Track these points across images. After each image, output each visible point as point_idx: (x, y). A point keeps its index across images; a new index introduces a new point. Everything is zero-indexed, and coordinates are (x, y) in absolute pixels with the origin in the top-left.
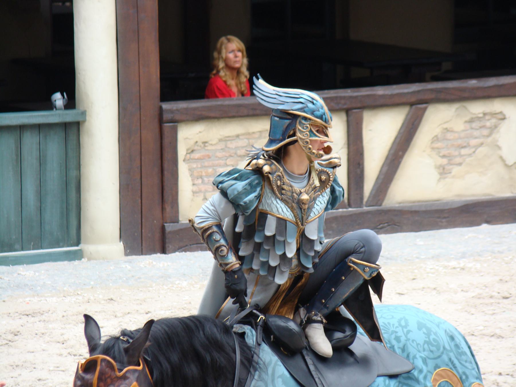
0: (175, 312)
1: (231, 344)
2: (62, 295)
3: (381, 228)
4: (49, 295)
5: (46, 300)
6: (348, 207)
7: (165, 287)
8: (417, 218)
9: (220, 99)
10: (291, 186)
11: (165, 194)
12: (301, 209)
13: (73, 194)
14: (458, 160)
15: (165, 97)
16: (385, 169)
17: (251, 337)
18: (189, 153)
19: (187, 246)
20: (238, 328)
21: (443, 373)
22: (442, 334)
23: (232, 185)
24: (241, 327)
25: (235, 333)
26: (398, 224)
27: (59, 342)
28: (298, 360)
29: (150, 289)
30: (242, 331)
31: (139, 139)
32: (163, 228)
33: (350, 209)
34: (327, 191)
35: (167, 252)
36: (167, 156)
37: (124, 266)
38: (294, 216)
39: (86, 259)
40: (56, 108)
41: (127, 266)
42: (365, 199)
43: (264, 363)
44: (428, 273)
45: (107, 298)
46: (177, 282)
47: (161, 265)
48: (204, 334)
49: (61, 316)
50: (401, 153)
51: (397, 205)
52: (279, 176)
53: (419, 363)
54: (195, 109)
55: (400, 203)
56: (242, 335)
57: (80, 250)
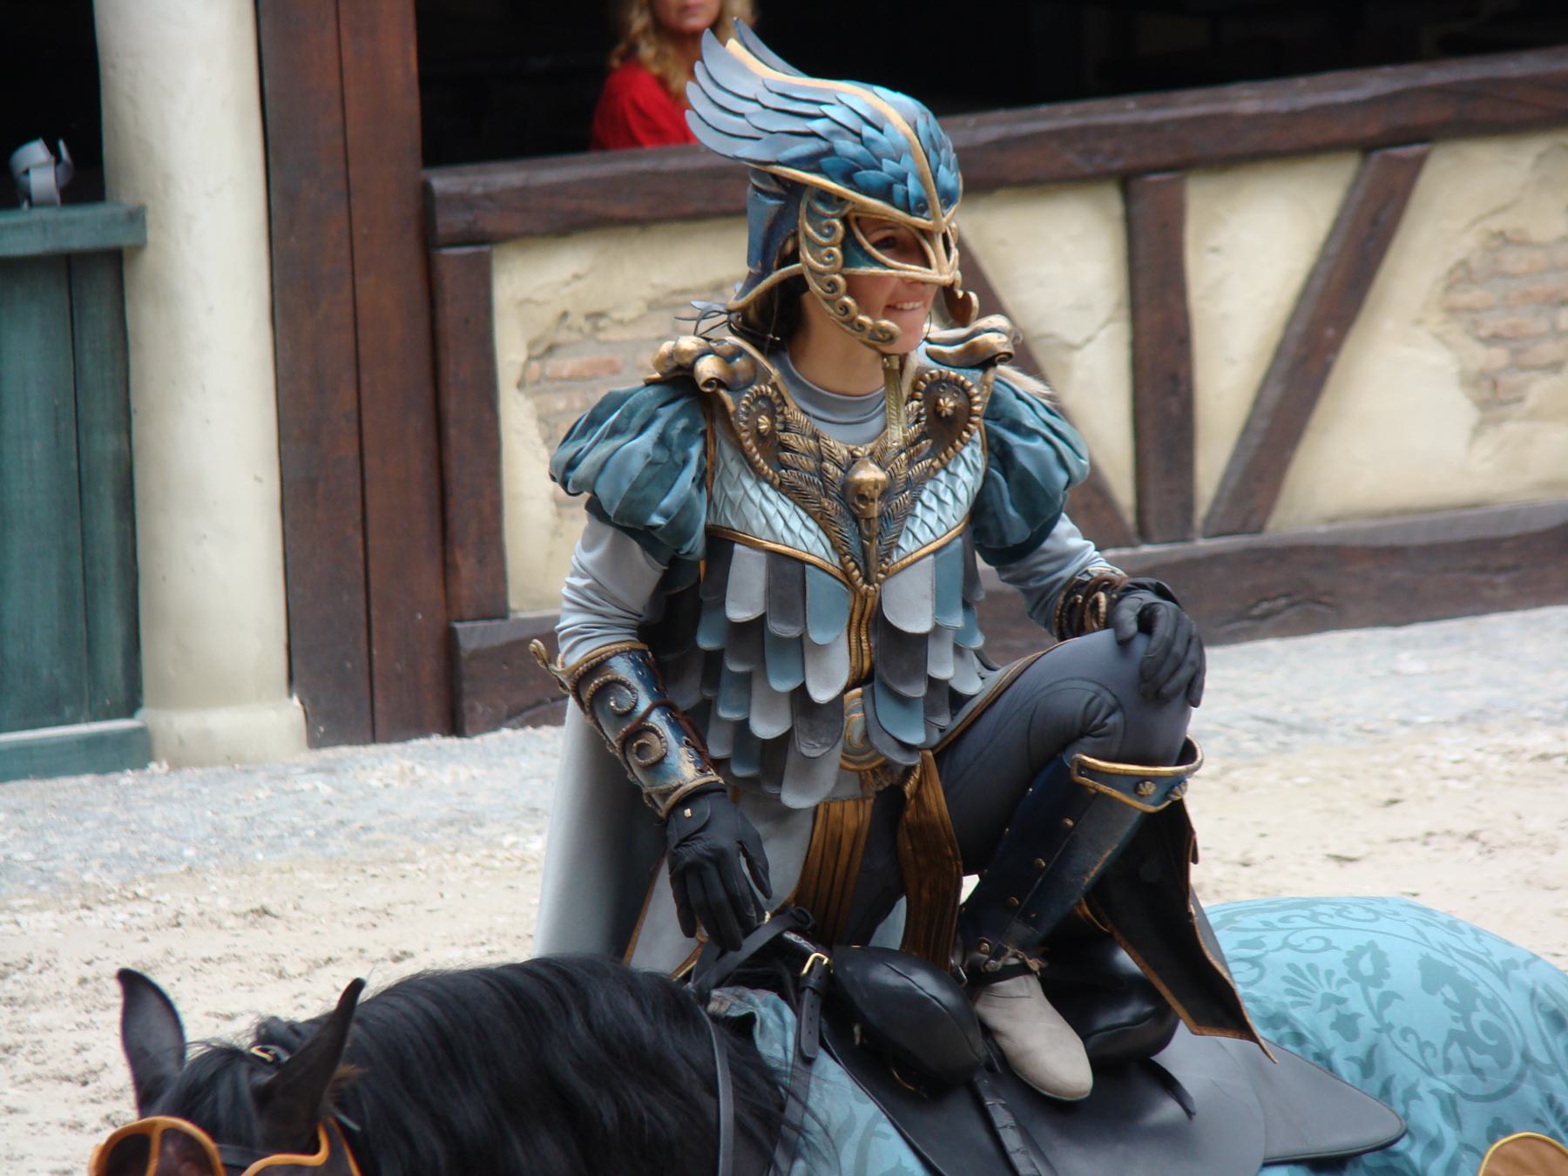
0: (504, 952)
1: (698, 1059)
2: (76, 902)
3: (1264, 617)
4: (28, 902)
5: (17, 923)
6: (1136, 540)
7: (467, 861)
8: (1397, 575)
9: (648, 148)
10: (816, 437)
11: (454, 513)
12: (856, 519)
13: (107, 524)
14: (1549, 350)
15: (442, 146)
16: (1275, 392)
17: (777, 1033)
18: (539, 358)
19: (539, 703)
20: (726, 1002)
21: (1524, 1155)
22: (1516, 1003)
23: (616, 450)
24: (740, 997)
25: (715, 1018)
26: (1326, 599)
27: (68, 1079)
28: (959, 1111)
29: (408, 867)
30: (743, 1012)
31: (348, 309)
32: (450, 641)
33: (1146, 549)
34: (966, 452)
35: (467, 728)
36: (456, 368)
37: (306, 786)
38: (833, 547)
39: (165, 766)
40: (28, 197)
41: (319, 784)
42: (1202, 510)
43: (826, 1131)
44: (1445, 778)
45: (244, 908)
46: (509, 840)
47: (447, 779)
48: (589, 1025)
49: (73, 982)
50: (1330, 332)
51: (1322, 529)
52: (763, 397)
53: (1429, 1116)
54: (553, 190)
55: (1332, 520)
56: (744, 1027)
57: (142, 731)
